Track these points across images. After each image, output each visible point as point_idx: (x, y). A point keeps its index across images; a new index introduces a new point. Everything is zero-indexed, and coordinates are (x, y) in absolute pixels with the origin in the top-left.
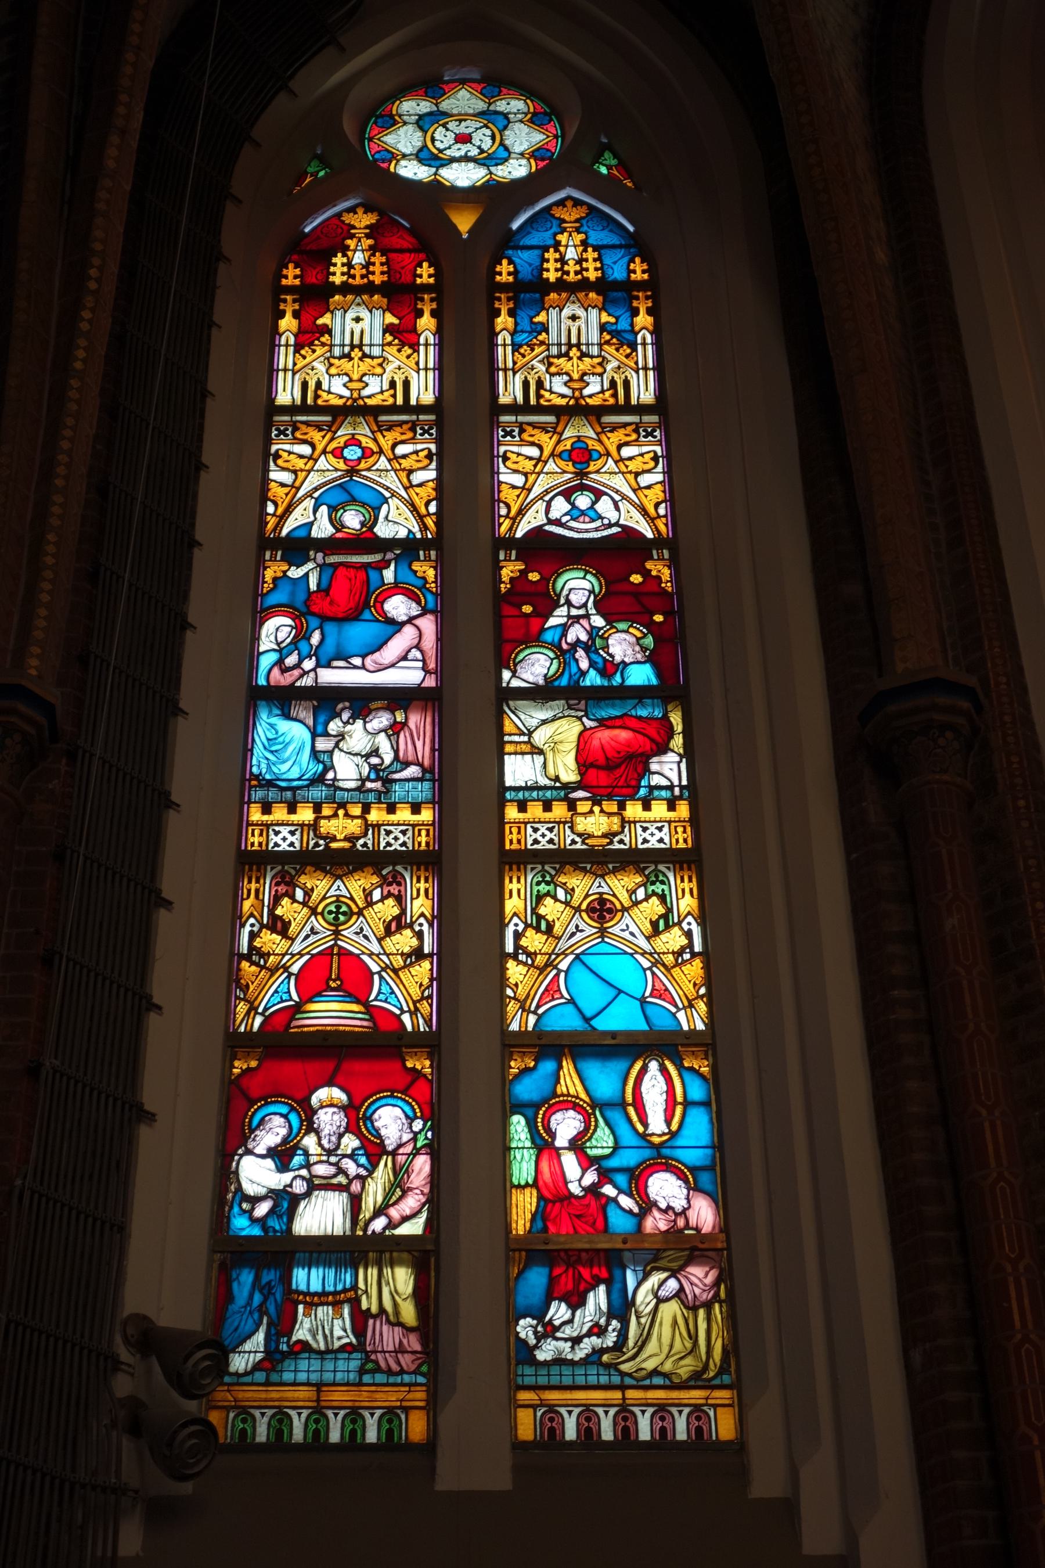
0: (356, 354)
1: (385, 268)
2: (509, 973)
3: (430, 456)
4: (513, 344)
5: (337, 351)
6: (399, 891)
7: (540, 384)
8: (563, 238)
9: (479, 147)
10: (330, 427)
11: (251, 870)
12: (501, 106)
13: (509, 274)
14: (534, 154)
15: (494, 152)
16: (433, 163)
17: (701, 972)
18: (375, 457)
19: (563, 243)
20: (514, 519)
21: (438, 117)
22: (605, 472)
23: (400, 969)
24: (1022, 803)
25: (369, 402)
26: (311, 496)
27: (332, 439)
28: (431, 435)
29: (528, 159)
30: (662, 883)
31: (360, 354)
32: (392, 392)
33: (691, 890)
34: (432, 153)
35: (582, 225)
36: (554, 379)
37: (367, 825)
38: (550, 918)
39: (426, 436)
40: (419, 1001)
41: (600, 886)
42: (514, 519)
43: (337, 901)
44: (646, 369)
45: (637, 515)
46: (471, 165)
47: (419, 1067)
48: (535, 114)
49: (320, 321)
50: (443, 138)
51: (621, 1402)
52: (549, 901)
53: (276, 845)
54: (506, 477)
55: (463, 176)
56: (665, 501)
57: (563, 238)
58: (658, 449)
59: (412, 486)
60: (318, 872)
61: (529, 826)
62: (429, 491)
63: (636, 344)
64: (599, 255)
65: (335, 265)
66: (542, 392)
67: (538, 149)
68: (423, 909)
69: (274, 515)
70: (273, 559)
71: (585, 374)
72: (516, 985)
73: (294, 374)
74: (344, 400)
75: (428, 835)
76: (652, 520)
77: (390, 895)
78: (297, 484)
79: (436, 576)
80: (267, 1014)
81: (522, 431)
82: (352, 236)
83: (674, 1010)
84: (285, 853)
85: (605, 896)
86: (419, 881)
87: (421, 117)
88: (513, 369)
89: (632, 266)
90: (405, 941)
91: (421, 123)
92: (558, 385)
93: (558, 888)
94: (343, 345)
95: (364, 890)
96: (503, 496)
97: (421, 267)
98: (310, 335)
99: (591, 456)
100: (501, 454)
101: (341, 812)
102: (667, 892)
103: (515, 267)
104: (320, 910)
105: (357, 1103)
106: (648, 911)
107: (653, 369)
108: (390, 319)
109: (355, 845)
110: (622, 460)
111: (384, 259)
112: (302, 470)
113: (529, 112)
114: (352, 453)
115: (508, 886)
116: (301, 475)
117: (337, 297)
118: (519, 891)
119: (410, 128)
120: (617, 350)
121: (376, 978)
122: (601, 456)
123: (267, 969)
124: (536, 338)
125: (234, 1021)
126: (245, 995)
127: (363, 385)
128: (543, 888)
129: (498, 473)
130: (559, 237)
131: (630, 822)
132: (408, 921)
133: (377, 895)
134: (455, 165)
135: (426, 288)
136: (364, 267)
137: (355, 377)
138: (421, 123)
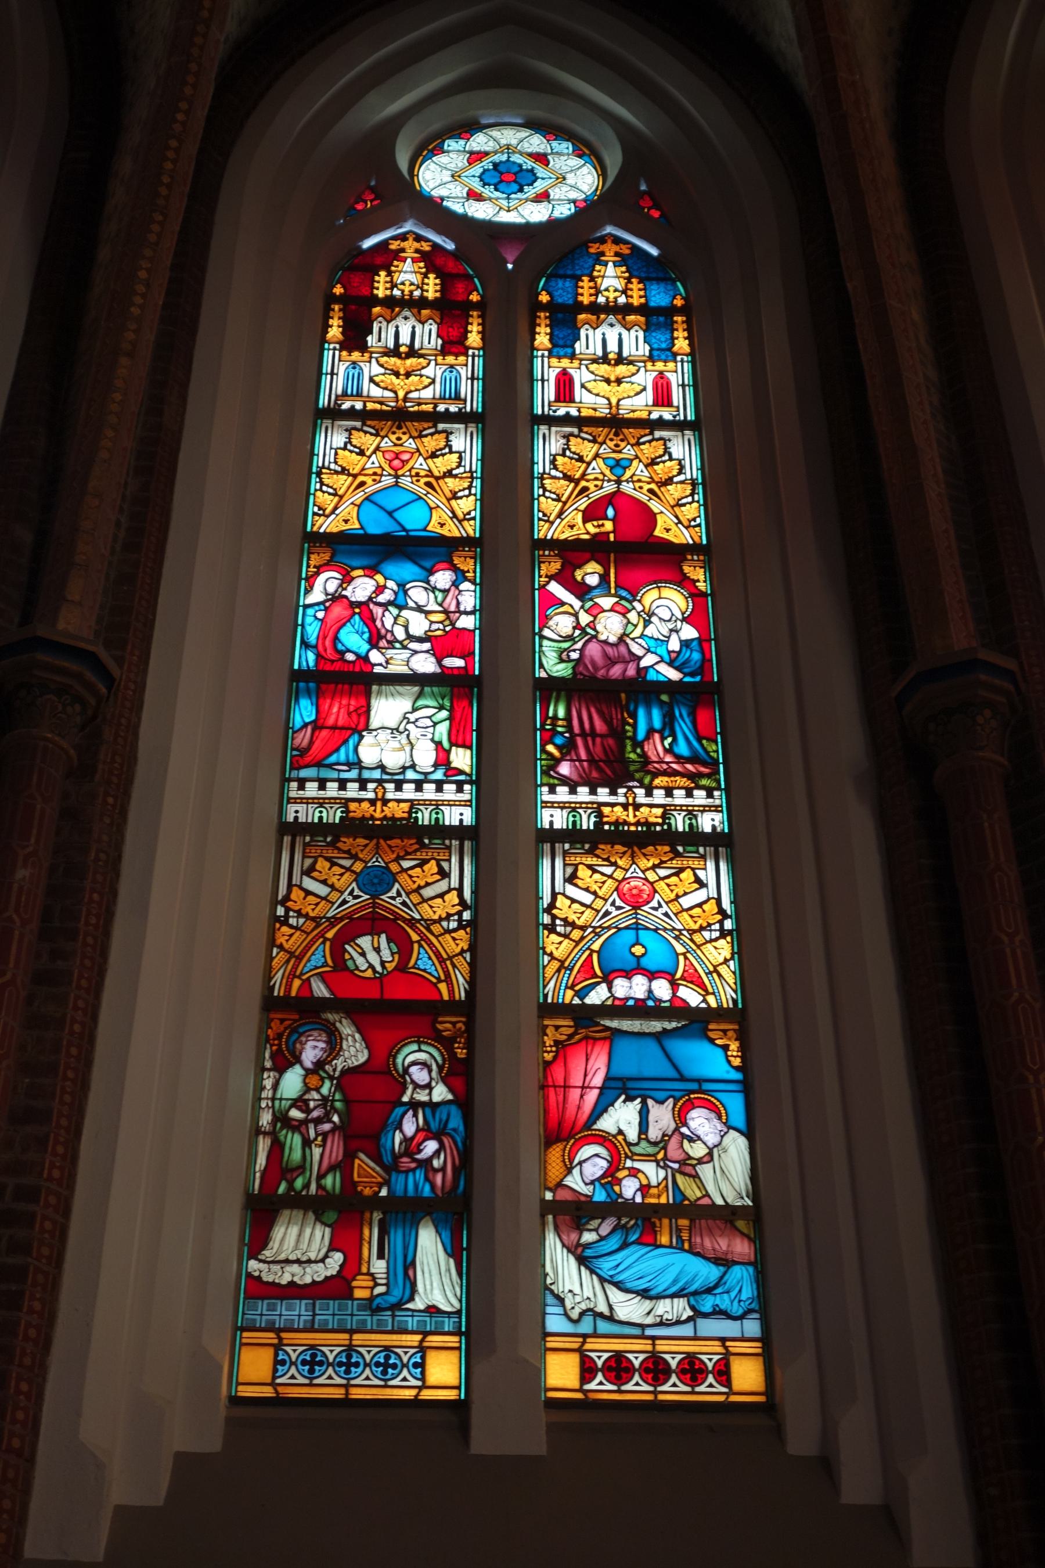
24: (110, 800)
51: (347, 1342)
98: (355, 339)
121: (416, 946)
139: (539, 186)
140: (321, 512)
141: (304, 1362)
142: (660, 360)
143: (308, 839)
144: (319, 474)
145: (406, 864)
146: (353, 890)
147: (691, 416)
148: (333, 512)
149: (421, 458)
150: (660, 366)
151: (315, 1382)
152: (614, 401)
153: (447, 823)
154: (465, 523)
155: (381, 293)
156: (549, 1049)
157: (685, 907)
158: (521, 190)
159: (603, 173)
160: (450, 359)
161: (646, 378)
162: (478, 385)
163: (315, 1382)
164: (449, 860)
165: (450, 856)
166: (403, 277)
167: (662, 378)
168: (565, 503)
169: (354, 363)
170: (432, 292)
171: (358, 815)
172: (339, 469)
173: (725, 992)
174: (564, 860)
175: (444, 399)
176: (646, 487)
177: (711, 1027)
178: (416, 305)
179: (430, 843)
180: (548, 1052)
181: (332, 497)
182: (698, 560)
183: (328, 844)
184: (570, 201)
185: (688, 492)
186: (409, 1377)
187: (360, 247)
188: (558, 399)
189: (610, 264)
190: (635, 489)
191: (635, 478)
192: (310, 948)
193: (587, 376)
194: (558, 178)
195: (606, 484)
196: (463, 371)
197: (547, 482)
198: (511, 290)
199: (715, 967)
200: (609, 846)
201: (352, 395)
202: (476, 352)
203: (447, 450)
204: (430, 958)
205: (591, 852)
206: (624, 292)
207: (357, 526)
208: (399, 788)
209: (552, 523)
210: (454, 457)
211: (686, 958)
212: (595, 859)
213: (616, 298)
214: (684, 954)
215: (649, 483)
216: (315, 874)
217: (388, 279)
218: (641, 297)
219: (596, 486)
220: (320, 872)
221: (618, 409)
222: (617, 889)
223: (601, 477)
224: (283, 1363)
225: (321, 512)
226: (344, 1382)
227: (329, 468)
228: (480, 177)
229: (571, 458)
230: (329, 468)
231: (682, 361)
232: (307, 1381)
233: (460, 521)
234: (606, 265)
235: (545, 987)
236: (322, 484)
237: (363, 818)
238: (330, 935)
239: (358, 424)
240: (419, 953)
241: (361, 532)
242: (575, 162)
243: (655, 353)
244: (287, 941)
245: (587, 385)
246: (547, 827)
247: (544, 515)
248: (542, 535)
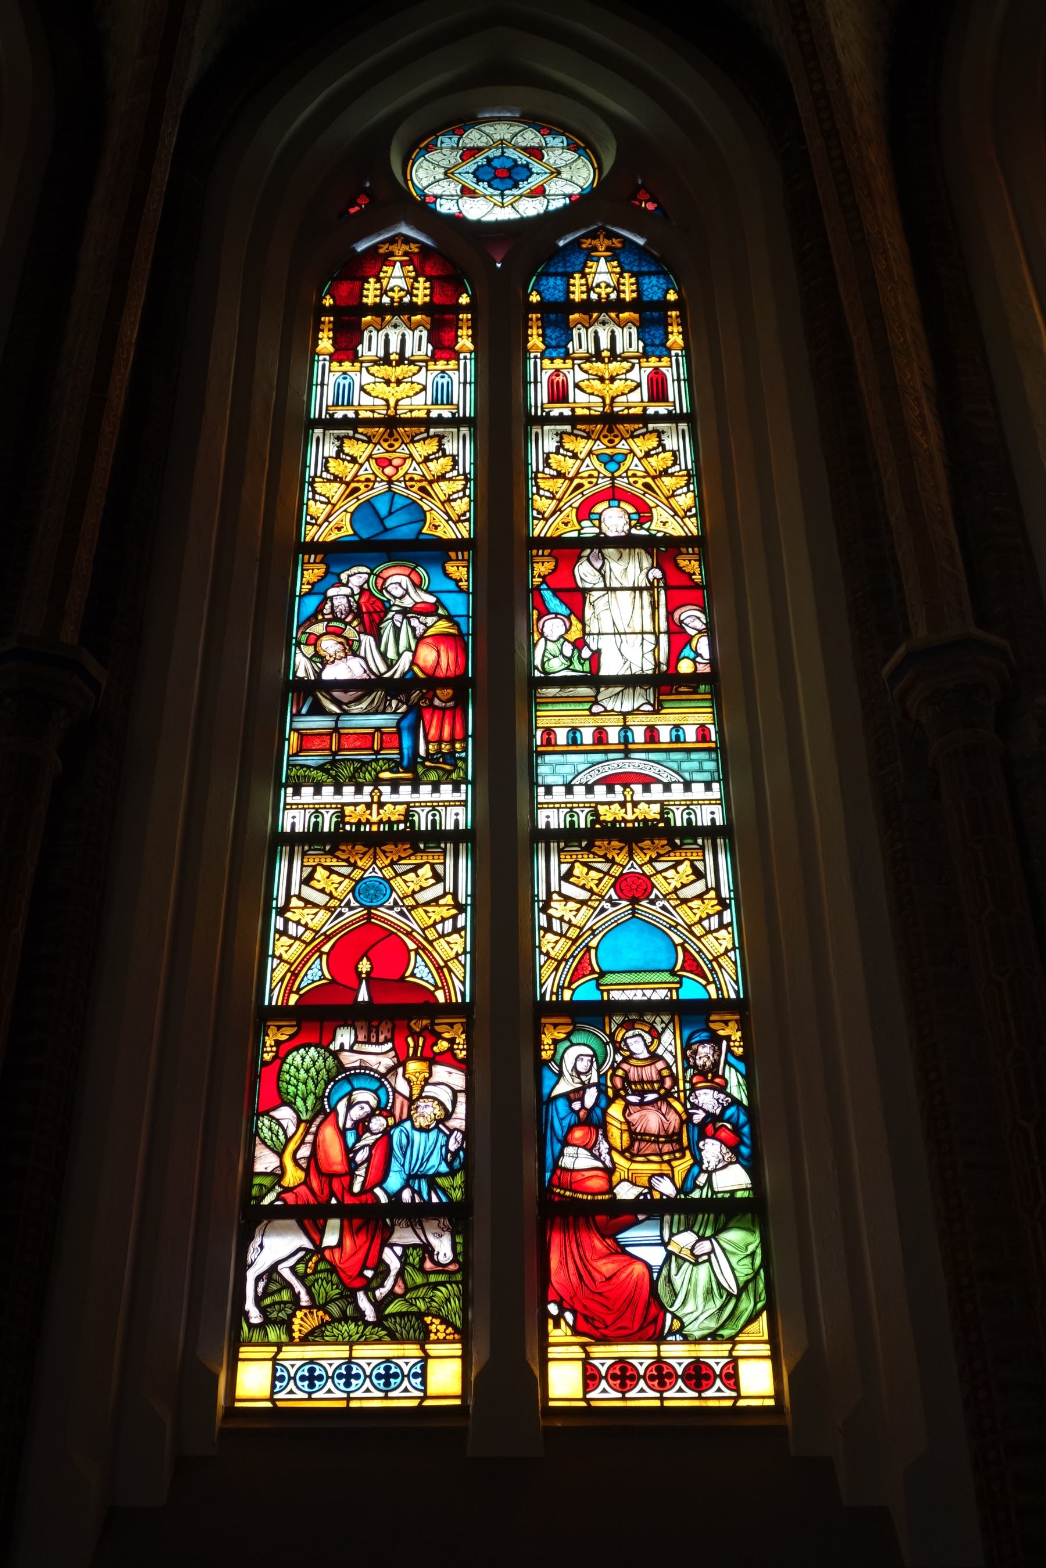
1: (634, 287)
51: (655, 1354)
83: (704, 982)
98: (346, 349)
121: (413, 954)
139: (534, 181)
140: (313, 521)
141: (379, 1376)
142: (441, 359)
143: (562, 845)
144: (312, 484)
145: (660, 866)
146: (349, 901)
147: (470, 412)
148: (326, 520)
149: (636, 460)
150: (653, 362)
151: (390, 1394)
152: (392, 404)
153: (699, 824)
154: (460, 525)
155: (370, 300)
156: (269, 1049)
157: (421, 901)
158: (516, 186)
159: (599, 169)
160: (441, 365)
161: (641, 374)
162: (470, 390)
163: (390, 1394)
164: (444, 864)
165: (445, 859)
166: (599, 278)
167: (656, 373)
168: (560, 500)
169: (345, 373)
170: (422, 296)
171: (609, 818)
172: (329, 477)
173: (730, 984)
174: (302, 862)
175: (337, 405)
176: (641, 481)
177: (712, 1018)
178: (405, 310)
179: (682, 844)
180: (461, 1050)
181: (550, 501)
182: (694, 554)
183: (583, 849)
184: (565, 196)
185: (683, 483)
186: (410, 1388)
187: (354, 250)
188: (551, 401)
189: (602, 260)
190: (629, 484)
191: (630, 473)
192: (308, 960)
193: (580, 376)
194: (552, 173)
195: (600, 481)
196: (455, 376)
197: (542, 484)
198: (498, 291)
199: (446, 962)
200: (606, 843)
201: (343, 405)
202: (468, 355)
203: (660, 449)
204: (426, 966)
205: (332, 853)
206: (410, 293)
207: (351, 532)
208: (646, 789)
209: (320, 526)
210: (669, 455)
211: (685, 950)
212: (591, 856)
213: (401, 298)
214: (682, 945)
215: (644, 477)
216: (572, 880)
217: (583, 281)
218: (633, 291)
219: (590, 483)
220: (319, 881)
221: (396, 409)
222: (353, 890)
223: (372, 477)
224: (281, 1379)
225: (313, 521)
226: (345, 1395)
227: (321, 477)
228: (532, 173)
229: (565, 456)
230: (321, 477)
231: (465, 358)
232: (382, 1395)
233: (455, 523)
234: (598, 261)
235: (542, 985)
236: (314, 492)
237: (615, 821)
238: (326, 948)
239: (568, 428)
240: (416, 962)
241: (355, 538)
242: (570, 156)
243: (649, 349)
244: (553, 948)
245: (581, 384)
246: (289, 830)
247: (539, 513)
248: (536, 533)
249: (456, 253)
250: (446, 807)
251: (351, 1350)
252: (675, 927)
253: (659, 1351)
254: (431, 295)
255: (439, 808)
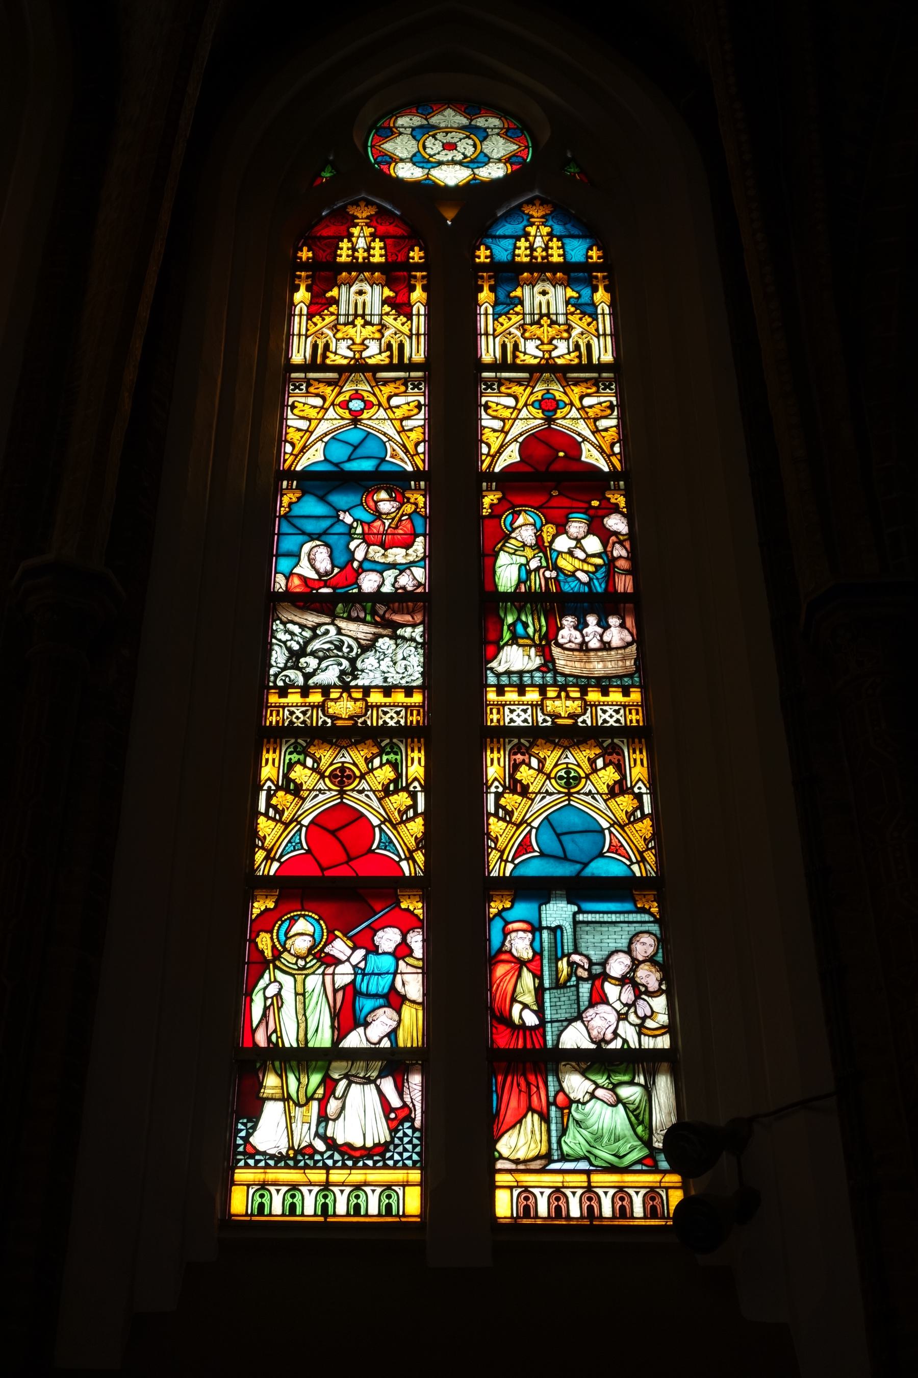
0: (359, 321)
2: (260, 826)
3: (419, 406)
4: (493, 314)
5: (342, 319)
6: (619, 760)
7: (516, 347)
8: (532, 230)
9: (463, 154)
10: (529, 382)
11: (413, 742)
12: (480, 122)
13: (486, 257)
14: (507, 160)
15: (476, 158)
16: (424, 165)
17: (422, 828)
18: (568, 407)
19: (356, 234)
20: (296, 456)
21: (429, 130)
22: (377, 419)
23: (398, 824)
25: (560, 361)
26: (321, 440)
27: (532, 393)
28: (612, 389)
29: (505, 164)
30: (396, 754)
31: (362, 322)
32: (577, 353)
33: (642, 760)
34: (424, 157)
35: (547, 221)
36: (528, 343)
37: (368, 707)
38: (525, 782)
39: (416, 390)
40: (414, 851)
41: (567, 757)
42: (493, 456)
43: (567, 768)
44: (605, 335)
45: (596, 453)
46: (458, 167)
47: (411, 908)
48: (508, 130)
49: (329, 294)
50: (433, 147)
51: (586, 1184)
52: (298, 768)
53: (605, 721)
54: (486, 421)
55: (452, 176)
56: (424, 441)
57: (532, 230)
58: (422, 399)
59: (404, 430)
60: (548, 744)
61: (506, 708)
62: (612, 434)
63: (597, 314)
64: (563, 244)
65: (342, 249)
66: (518, 353)
67: (514, 155)
68: (640, 775)
69: (291, 454)
70: (489, 489)
71: (553, 338)
72: (265, 837)
73: (494, 338)
74: (538, 360)
75: (418, 714)
76: (608, 457)
77: (611, 763)
78: (506, 429)
79: (425, 503)
80: (282, 860)
81: (309, 385)
82: (355, 225)
83: (628, 863)
84: (519, 728)
85: (346, 765)
86: (634, 752)
87: (413, 129)
88: (493, 335)
89: (590, 253)
90: (402, 799)
91: (414, 133)
92: (531, 347)
93: (532, 758)
94: (534, 314)
95: (589, 759)
96: (289, 437)
97: (413, 251)
99: (558, 404)
100: (290, 403)
101: (563, 694)
102: (399, 761)
103: (491, 252)
104: (553, 775)
105: (331, 935)
106: (382, 777)
107: (611, 335)
108: (387, 292)
109: (577, 722)
110: (391, 408)
111: (560, 244)
112: (509, 419)
113: (504, 128)
114: (356, 405)
115: (265, 756)
116: (314, 423)
117: (525, 274)
118: (274, 760)
119: (405, 138)
120: (395, 319)
121: (377, 830)
122: (566, 405)
123: (513, 823)
124: (513, 309)
125: (489, 866)
126: (496, 845)
127: (553, 347)
128: (295, 757)
129: (481, 419)
130: (529, 229)
131: (591, 706)
132: (629, 785)
133: (600, 763)
134: (444, 167)
135: (417, 267)
136: (365, 251)
137: (358, 341)
138: (414, 133)
249: (415, 212)
250: (404, 1186)
251: (328, 1174)
252: (516, 550)
253: (589, 1181)
254: (386, 255)
255: (396, 1188)
